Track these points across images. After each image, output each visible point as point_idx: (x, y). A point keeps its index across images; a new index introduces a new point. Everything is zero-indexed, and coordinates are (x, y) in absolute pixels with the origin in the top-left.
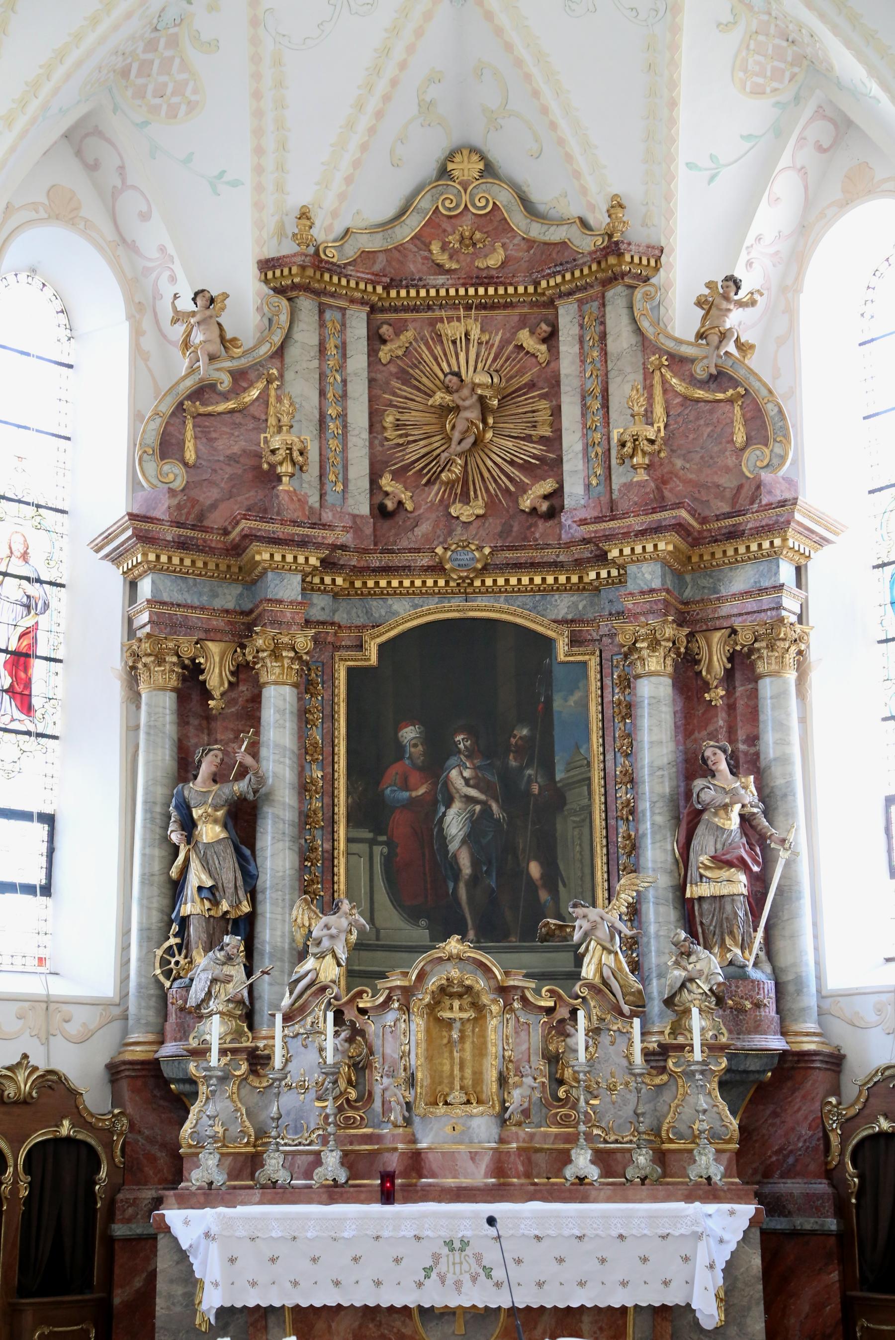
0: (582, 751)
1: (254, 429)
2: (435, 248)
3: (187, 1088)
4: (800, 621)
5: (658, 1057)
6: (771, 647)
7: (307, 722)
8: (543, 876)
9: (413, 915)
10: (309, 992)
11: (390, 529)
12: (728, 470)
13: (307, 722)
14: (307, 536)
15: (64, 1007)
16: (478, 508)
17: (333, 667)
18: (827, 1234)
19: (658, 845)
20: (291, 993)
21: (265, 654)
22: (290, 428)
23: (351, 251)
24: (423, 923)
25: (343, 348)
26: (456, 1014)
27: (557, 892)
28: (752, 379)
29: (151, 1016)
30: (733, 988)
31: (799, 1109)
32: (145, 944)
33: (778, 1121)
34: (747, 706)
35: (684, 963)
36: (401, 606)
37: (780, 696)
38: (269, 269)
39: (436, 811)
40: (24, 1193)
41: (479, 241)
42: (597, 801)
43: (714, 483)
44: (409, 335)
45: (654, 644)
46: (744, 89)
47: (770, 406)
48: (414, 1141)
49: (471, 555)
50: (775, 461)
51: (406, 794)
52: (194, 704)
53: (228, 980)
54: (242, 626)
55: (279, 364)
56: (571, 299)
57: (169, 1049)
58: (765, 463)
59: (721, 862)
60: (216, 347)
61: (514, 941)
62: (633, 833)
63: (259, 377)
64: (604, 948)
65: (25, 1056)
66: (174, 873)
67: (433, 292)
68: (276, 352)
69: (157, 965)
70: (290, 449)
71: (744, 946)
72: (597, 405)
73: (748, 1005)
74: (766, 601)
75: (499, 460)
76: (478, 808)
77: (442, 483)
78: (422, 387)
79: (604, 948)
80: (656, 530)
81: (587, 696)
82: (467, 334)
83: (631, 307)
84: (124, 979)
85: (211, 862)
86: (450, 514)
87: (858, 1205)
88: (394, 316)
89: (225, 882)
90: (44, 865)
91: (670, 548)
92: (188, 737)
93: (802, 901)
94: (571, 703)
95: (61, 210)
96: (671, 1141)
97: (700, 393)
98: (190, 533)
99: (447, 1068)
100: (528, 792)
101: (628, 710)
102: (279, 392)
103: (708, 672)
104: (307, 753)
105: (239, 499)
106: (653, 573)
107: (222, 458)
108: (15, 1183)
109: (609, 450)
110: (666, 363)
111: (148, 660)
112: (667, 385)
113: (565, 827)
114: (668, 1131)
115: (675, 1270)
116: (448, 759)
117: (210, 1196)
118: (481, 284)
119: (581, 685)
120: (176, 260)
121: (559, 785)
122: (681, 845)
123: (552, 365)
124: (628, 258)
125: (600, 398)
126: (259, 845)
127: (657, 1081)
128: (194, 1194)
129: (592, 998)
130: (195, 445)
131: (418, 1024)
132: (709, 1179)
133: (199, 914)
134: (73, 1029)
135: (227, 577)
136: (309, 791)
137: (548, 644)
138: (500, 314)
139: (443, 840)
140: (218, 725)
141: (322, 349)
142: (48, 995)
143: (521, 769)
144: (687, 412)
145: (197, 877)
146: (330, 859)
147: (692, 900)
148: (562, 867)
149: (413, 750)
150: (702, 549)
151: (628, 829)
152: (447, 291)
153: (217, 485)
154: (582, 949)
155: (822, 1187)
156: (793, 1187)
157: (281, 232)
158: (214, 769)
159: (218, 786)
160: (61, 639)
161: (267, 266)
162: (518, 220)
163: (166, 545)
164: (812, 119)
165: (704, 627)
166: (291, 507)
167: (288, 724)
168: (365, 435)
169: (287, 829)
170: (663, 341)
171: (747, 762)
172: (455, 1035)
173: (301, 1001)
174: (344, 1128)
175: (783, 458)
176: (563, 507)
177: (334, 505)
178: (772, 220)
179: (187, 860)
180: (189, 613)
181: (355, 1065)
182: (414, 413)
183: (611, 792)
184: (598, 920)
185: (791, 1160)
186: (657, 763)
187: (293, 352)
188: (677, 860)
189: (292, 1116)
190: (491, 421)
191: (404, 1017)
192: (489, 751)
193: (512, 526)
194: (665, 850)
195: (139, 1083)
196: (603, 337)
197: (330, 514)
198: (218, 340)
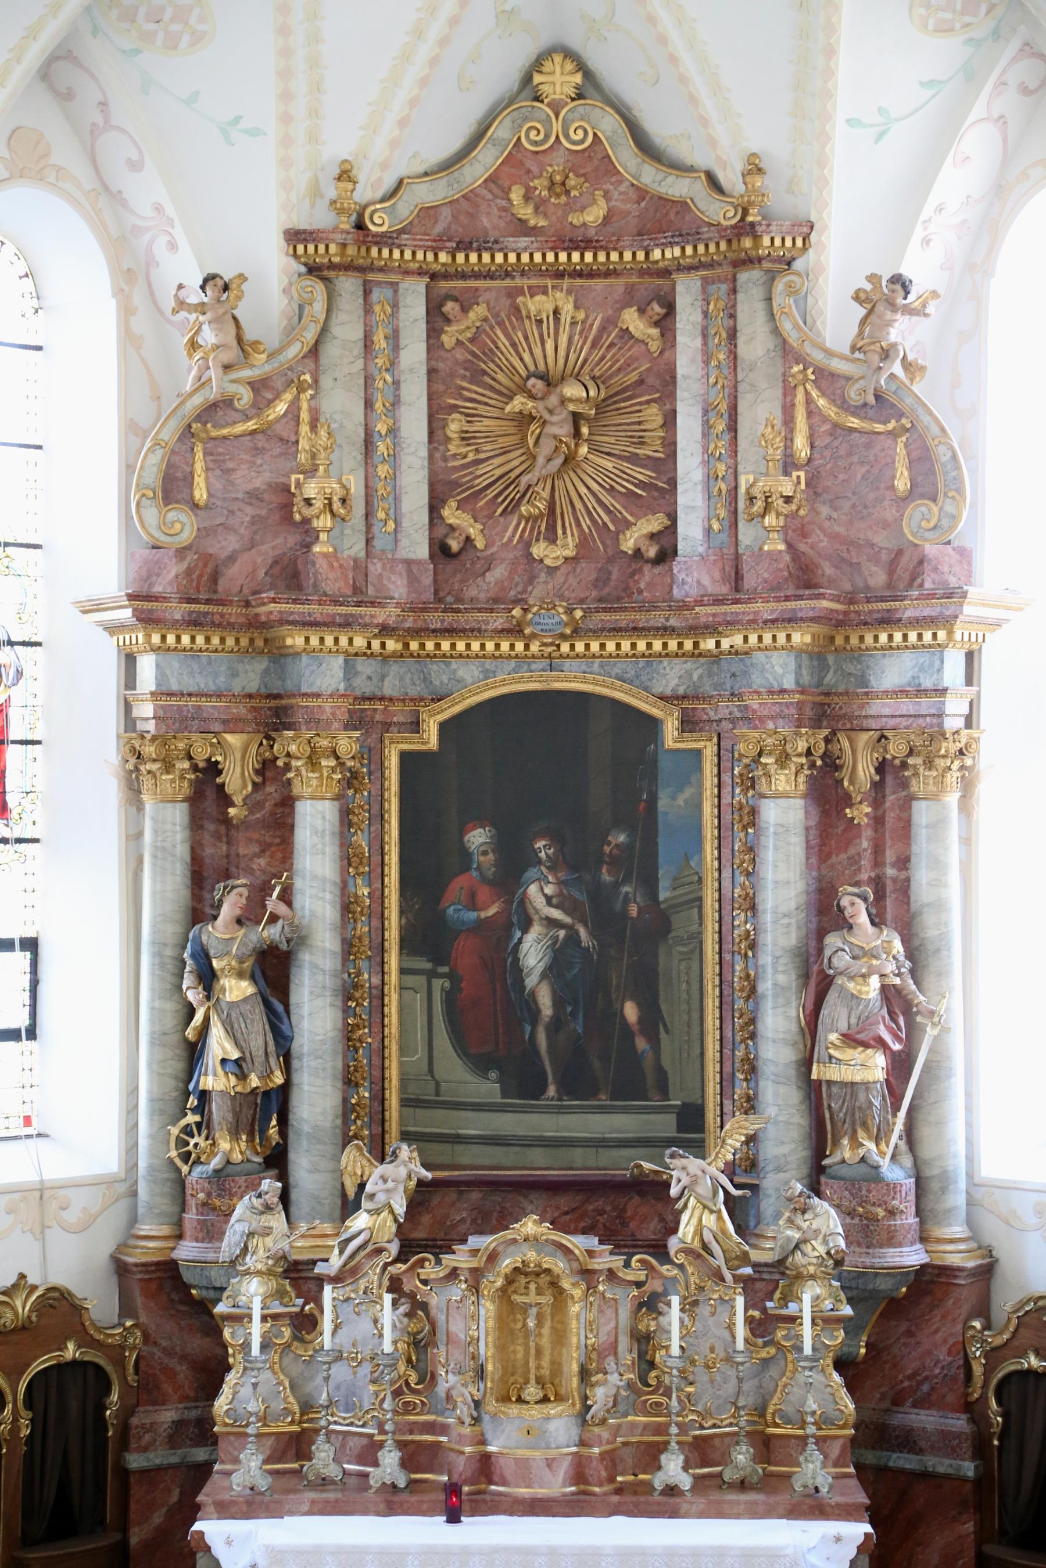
0: (692, 864)
1: (280, 454)
2: (516, 195)
3: (211, 1294)
4: (969, 724)
6: (929, 764)
7: (350, 825)
8: (641, 1020)
9: (481, 1064)
10: (362, 1254)
11: (454, 573)
12: (885, 525)
13: (350, 825)
14: (352, 615)
15: (62, 1193)
16: (567, 546)
17: (382, 752)
18: (964, 1480)
19: (780, 1010)
20: (341, 1252)
21: (299, 763)
22: (332, 478)
23: (406, 207)
24: (493, 1075)
25: (394, 338)
26: (532, 1298)
27: (659, 1040)
28: (920, 411)
29: (166, 1205)
30: (864, 1192)
31: (936, 1331)
32: (156, 1118)
33: (912, 1341)
34: (899, 819)
35: (799, 1220)
36: (468, 672)
37: (939, 824)
38: (300, 241)
39: (509, 936)
40: (25, 1432)
41: (574, 188)
42: (710, 928)
43: (867, 541)
44: (479, 311)
45: (783, 760)
46: (926, 27)
47: (942, 449)
48: (483, 1442)
49: (557, 619)
50: (945, 523)
51: (472, 915)
52: (210, 804)
53: (267, 1232)
55: (312, 366)
56: (692, 274)
58: (932, 524)
59: (850, 1040)
60: (232, 354)
61: (603, 1100)
62: (752, 973)
63: (289, 383)
64: (705, 1207)
65: (22, 1276)
66: (190, 1034)
67: (512, 258)
68: (310, 351)
69: (173, 1144)
70: (330, 499)
72: (721, 426)
73: (881, 1212)
74: (925, 705)
75: (595, 487)
76: (562, 933)
77: (521, 516)
78: (498, 387)
79: (705, 1207)
80: (791, 620)
81: (701, 794)
82: (556, 312)
83: (769, 299)
84: (131, 1148)
85: (236, 1026)
86: (531, 554)
87: (1000, 1448)
88: (460, 284)
89: (253, 1050)
90: (27, 1002)
91: (808, 639)
92: (202, 845)
93: (952, 1080)
94: (680, 802)
96: (777, 1426)
97: (854, 422)
98: (203, 608)
99: (520, 1356)
100: (624, 914)
102: (313, 403)
103: (852, 782)
104: (350, 865)
105: (263, 548)
106: (784, 666)
107: (240, 496)
108: (15, 1420)
109: (736, 488)
110: (813, 377)
111: (154, 767)
112: (812, 406)
113: (670, 960)
114: (773, 1414)
116: (526, 870)
117: (252, 1506)
118: (576, 249)
119: (693, 779)
120: (177, 223)
121: (662, 906)
122: (807, 1012)
123: (667, 354)
124: (766, 241)
125: (726, 416)
126: (293, 999)
127: (763, 1354)
128: (235, 1503)
129: (690, 1264)
130: (207, 479)
131: (488, 1308)
132: (817, 1490)
134: (72, 1216)
135: (251, 651)
136: (354, 913)
137: (653, 725)
138: (599, 284)
139: (518, 971)
140: (240, 836)
142: (42, 1182)
143: (616, 885)
144: (836, 443)
145: (219, 1045)
147: (819, 1082)
148: (664, 1007)
149: (482, 858)
150: (849, 631)
151: (746, 967)
152: (531, 255)
153: (235, 531)
154: (679, 1205)
155: (959, 1423)
156: (925, 1420)
157: (315, 192)
158: (238, 912)
159: (243, 931)
160: (39, 714)
161: (295, 237)
162: (625, 157)
163: (174, 625)
164: (1014, 60)
165: (848, 726)
166: (331, 575)
167: (327, 849)
168: (424, 452)
169: (328, 981)
170: (809, 351)
171: (895, 891)
172: (531, 1323)
173: (353, 1263)
174: (403, 1414)
175: (955, 518)
176: (675, 553)
177: (383, 551)
178: (959, 182)
179: (207, 1020)
180: (204, 703)
181: (416, 1343)
182: (486, 422)
183: (727, 919)
184: (700, 1173)
185: (925, 1388)
186: (783, 909)
187: (331, 351)
188: (802, 1028)
189: (343, 1390)
190: (585, 430)
191: (473, 1298)
192: (577, 861)
193: (610, 573)
194: (788, 1018)
195: (154, 1286)
196: (733, 334)
197: (379, 566)
198: (234, 343)
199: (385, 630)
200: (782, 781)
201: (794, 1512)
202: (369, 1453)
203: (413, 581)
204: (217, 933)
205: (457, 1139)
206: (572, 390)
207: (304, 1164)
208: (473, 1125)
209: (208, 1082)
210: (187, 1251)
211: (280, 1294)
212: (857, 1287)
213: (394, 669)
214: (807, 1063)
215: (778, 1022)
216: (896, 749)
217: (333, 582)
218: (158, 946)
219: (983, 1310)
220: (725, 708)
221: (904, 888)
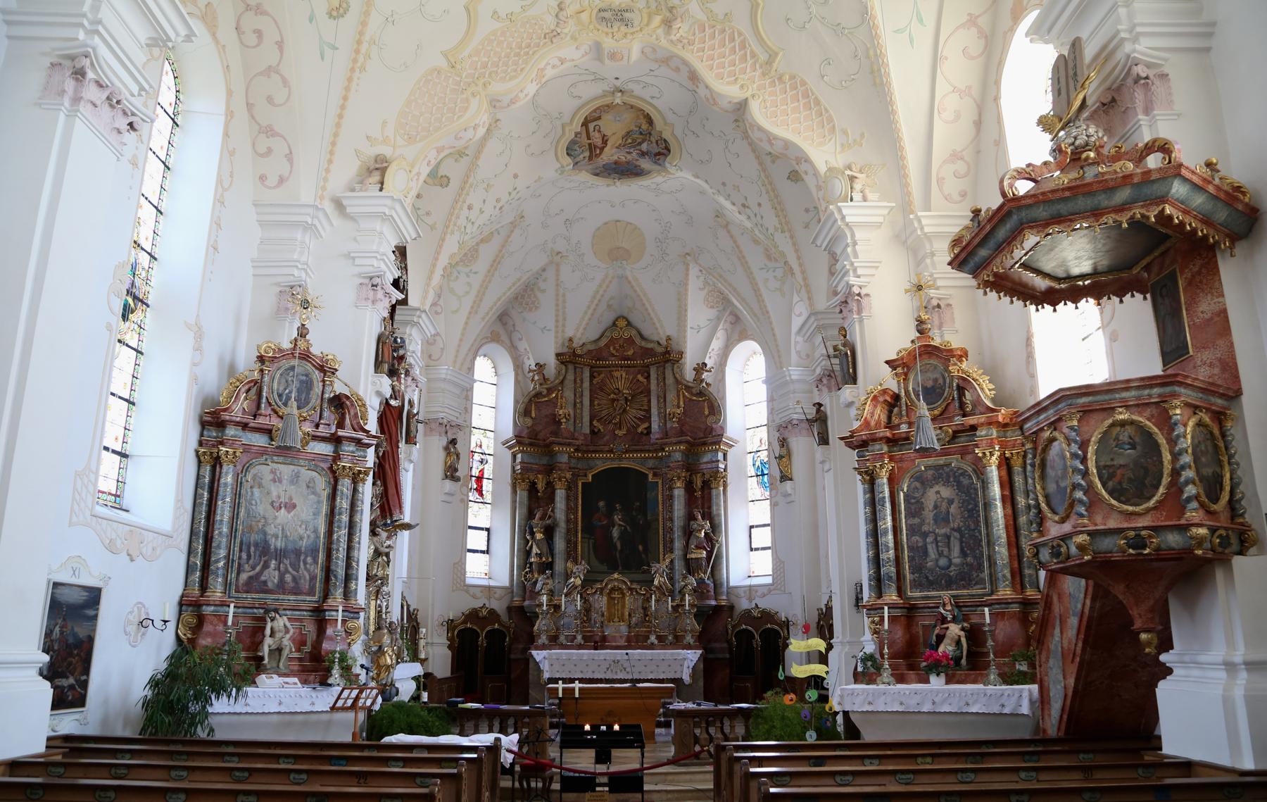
5: (675, 608)
23: (585, 350)
29: (521, 593)
36: (598, 462)
45: (679, 478)
54: (549, 469)
57: (527, 603)
59: (698, 547)
71: (705, 573)
80: (680, 443)
95: (494, 338)
101: (671, 497)
117: (543, 647)
131: (605, 598)
133: (534, 560)
145: (535, 550)
155: (725, 645)
156: (717, 645)
157: (563, 345)
162: (638, 340)
178: (717, 344)
187: (566, 382)
207: (559, 566)
215: (678, 544)
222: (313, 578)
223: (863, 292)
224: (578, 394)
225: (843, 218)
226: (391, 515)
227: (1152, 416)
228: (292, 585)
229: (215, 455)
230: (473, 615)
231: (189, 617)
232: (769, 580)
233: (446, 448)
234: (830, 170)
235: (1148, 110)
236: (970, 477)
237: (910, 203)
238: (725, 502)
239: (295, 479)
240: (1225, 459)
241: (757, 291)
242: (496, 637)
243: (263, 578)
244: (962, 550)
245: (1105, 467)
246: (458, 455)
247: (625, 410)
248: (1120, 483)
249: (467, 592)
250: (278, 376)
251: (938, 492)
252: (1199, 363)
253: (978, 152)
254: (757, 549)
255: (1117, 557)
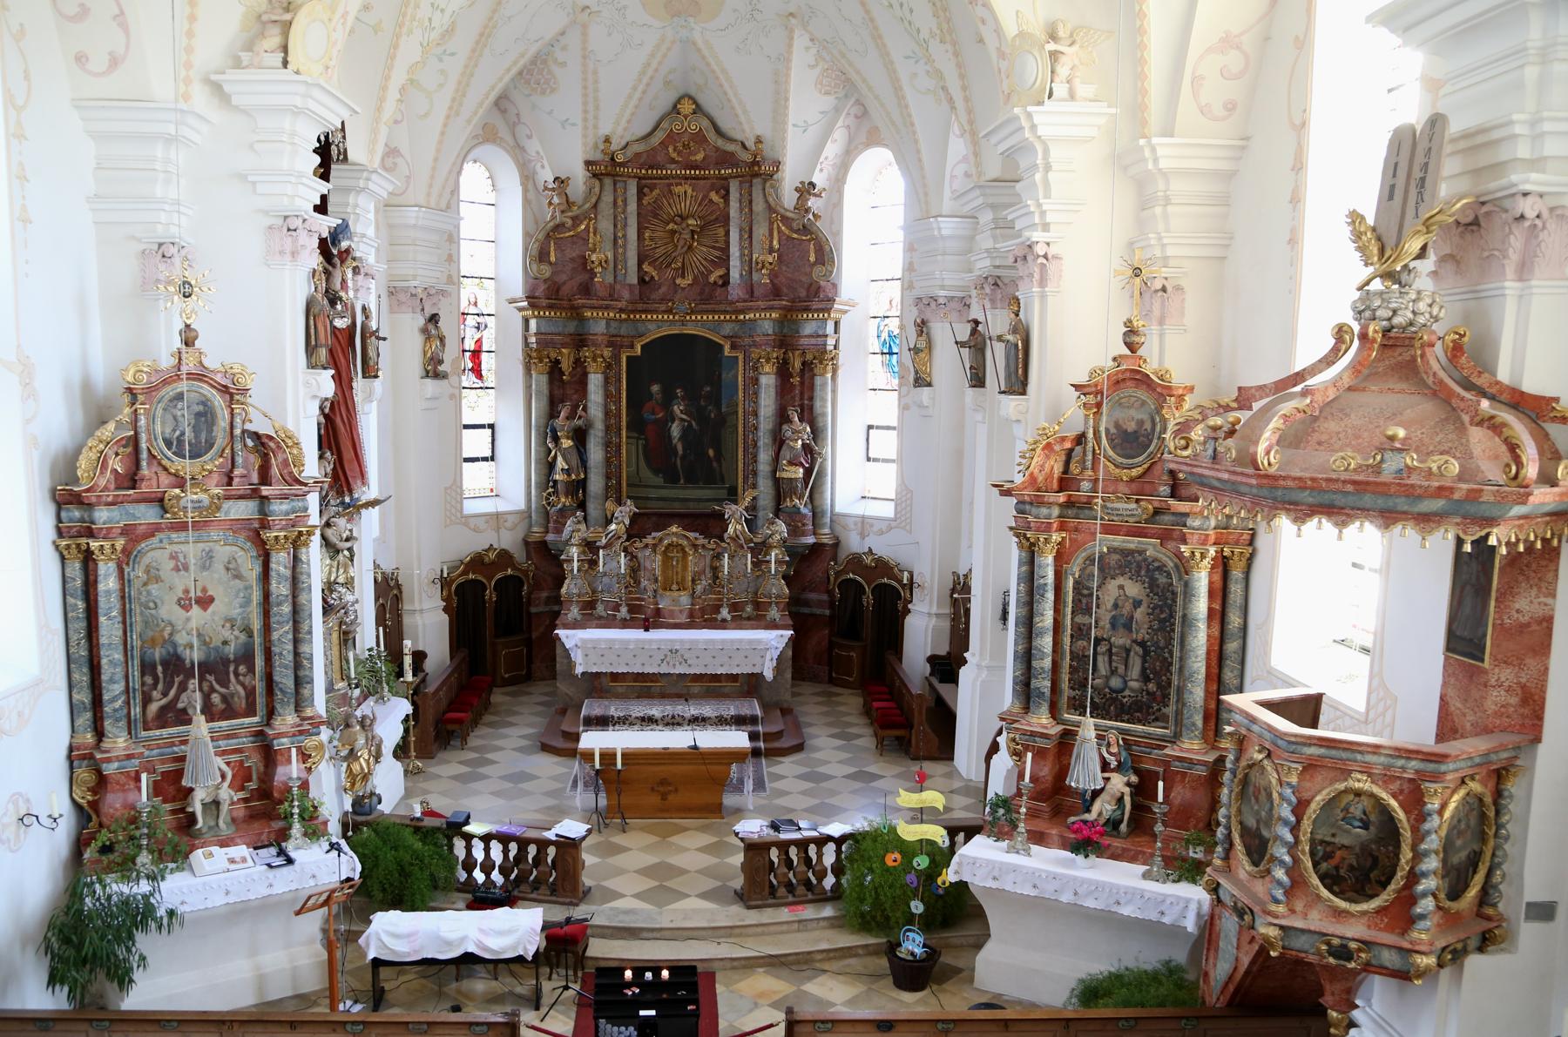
9: (656, 472)
23: (630, 152)
25: (625, 201)
36: (651, 326)
37: (824, 385)
45: (768, 360)
59: (791, 463)
60: (564, 207)
80: (771, 308)
95: (487, 135)
115: (758, 660)
117: (575, 625)
131: (659, 558)
133: (562, 492)
134: (508, 524)
135: (571, 318)
137: (721, 347)
138: (702, 182)
139: (670, 437)
141: (615, 203)
146: (619, 446)
155: (825, 597)
156: (813, 596)
157: (596, 146)
162: (711, 136)
178: (832, 150)
187: (602, 205)
192: (692, 398)
196: (751, 202)
199: (621, 311)
200: (767, 368)
201: (767, 627)
202: (617, 608)
203: (631, 292)
204: (559, 422)
205: (648, 498)
206: (691, 222)
207: (593, 508)
208: (653, 493)
209: (557, 477)
210: (550, 537)
211: (584, 553)
212: (791, 551)
213: (625, 325)
214: (775, 472)
215: (764, 457)
216: (809, 357)
217: (602, 293)
218: (537, 427)
219: (835, 558)
220: (747, 341)
221: (811, 408)
222: (250, 693)
223: (1052, 251)
224: (618, 223)
225: (1033, 127)
226: (350, 491)
227: (1401, 791)
228: (222, 706)
229: (84, 547)
230: (477, 562)
231: (84, 774)
232: (887, 510)
233: (425, 331)
234: (1021, 35)
235: (1524, 271)
236: (1169, 575)
237: (1144, 123)
238: (834, 391)
239: (207, 560)
240: (1491, 833)
241: (897, 89)
242: (510, 586)
243: (180, 705)
244: (1144, 670)
245: (1322, 842)
246: (442, 339)
247: (690, 247)
248: (1337, 868)
249: (466, 525)
250: (159, 412)
251: (1121, 587)
252: (1493, 682)
253: (1267, 39)
254: (875, 460)
255: (1312, 958)
